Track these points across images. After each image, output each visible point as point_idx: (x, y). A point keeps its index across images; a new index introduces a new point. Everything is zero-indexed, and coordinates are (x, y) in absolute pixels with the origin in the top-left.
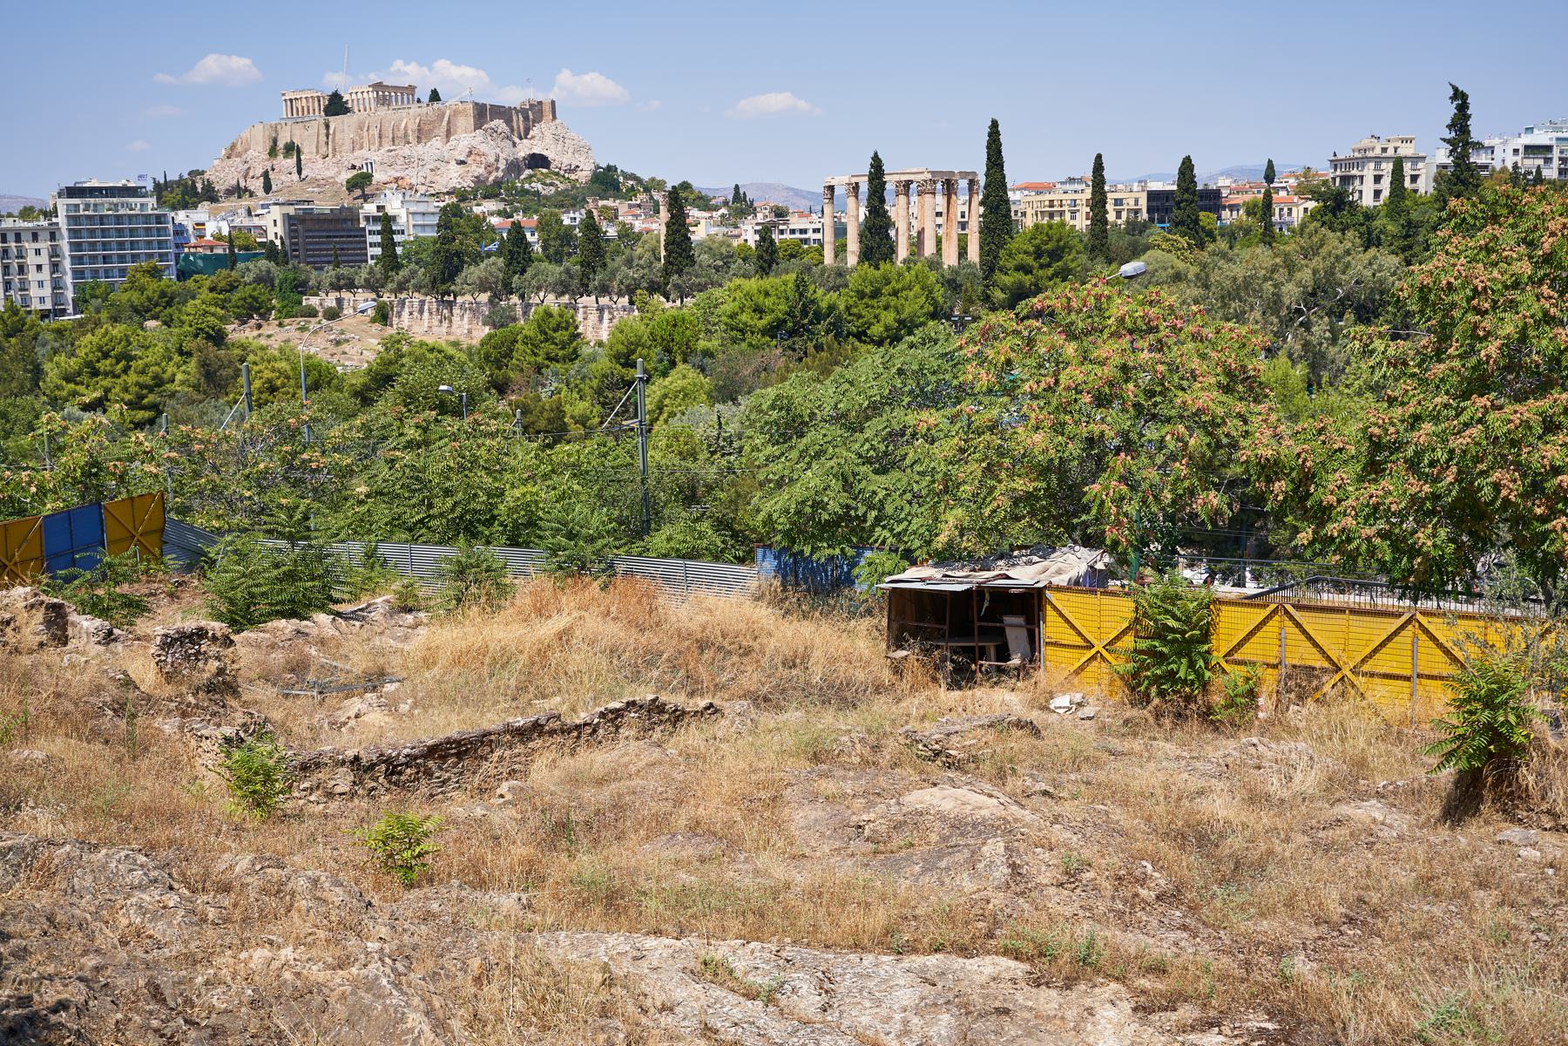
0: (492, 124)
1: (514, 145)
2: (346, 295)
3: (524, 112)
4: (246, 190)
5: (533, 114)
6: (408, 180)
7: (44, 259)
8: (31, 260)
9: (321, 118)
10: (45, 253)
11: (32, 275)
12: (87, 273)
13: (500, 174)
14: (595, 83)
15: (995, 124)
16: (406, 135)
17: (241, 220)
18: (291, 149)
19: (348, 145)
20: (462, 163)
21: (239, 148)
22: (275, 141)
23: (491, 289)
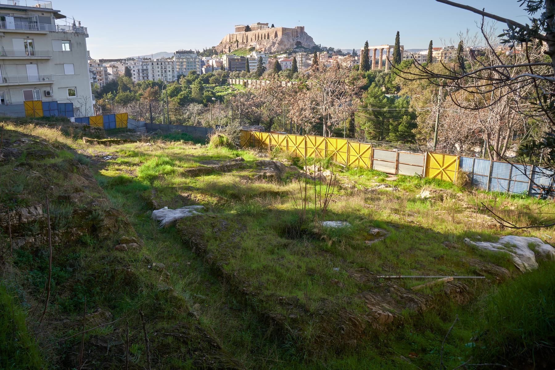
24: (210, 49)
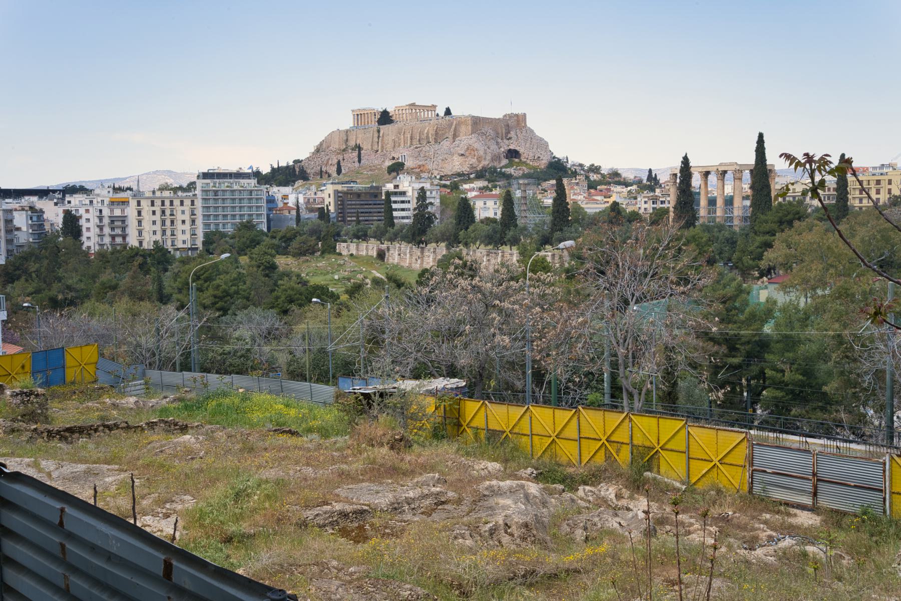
6: (427, 167)
7: (187, 217)
8: (179, 217)
11: (179, 227)
15: (761, 136)
16: (428, 137)
23: (447, 240)
24: (288, 167)
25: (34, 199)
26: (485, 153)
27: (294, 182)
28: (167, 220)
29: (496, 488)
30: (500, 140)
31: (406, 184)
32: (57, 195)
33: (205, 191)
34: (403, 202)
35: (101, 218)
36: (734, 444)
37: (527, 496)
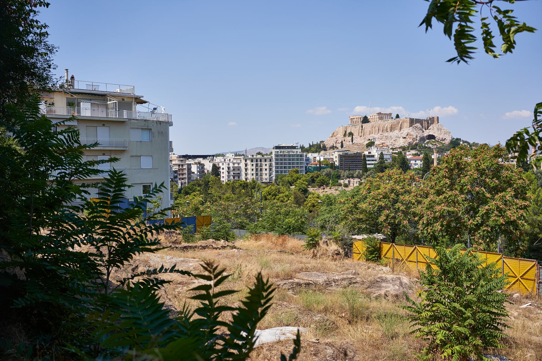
0: (416, 125)
1: (423, 132)
2: (352, 180)
3: (427, 121)
4: (336, 147)
5: (431, 121)
7: (267, 167)
8: (264, 167)
9: (360, 124)
10: (268, 165)
12: (279, 172)
13: (417, 141)
14: (451, 110)
16: (387, 129)
17: (327, 157)
18: (351, 134)
19: (368, 133)
20: (405, 138)
21: (335, 134)
22: (346, 132)
25: (201, 160)
26: (415, 133)
27: (320, 152)
28: (258, 170)
29: (384, 278)
30: (424, 130)
31: (375, 151)
32: (211, 158)
33: (277, 156)
34: (373, 160)
35: (229, 168)
36: (529, 268)
37: (401, 284)
